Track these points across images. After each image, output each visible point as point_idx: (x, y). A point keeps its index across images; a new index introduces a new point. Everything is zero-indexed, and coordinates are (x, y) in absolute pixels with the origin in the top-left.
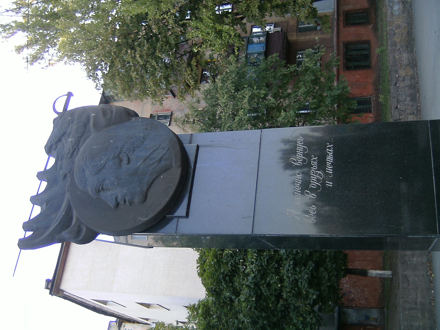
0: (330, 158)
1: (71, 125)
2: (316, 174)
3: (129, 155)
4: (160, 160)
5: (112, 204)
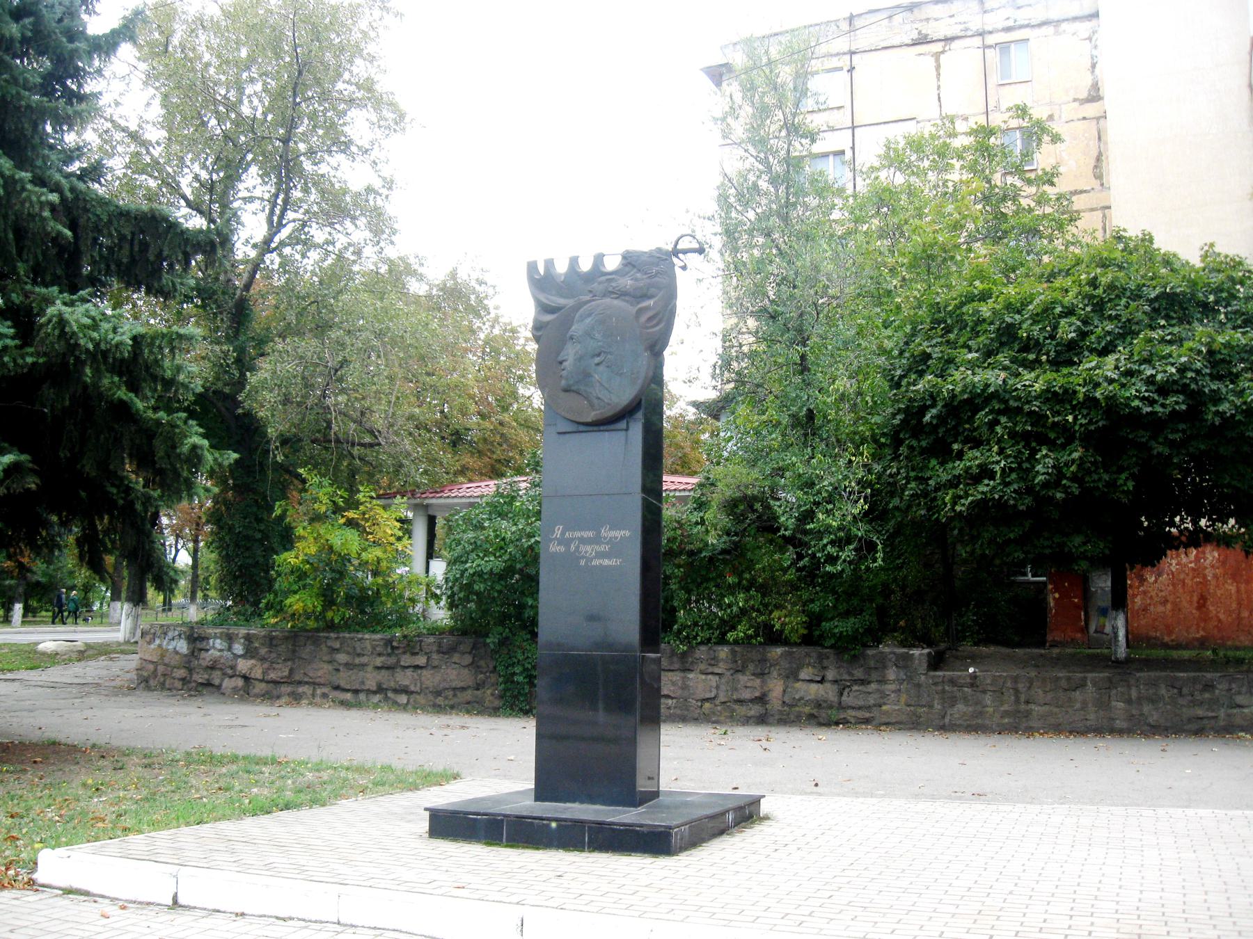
0: (606, 562)
5: (560, 359)
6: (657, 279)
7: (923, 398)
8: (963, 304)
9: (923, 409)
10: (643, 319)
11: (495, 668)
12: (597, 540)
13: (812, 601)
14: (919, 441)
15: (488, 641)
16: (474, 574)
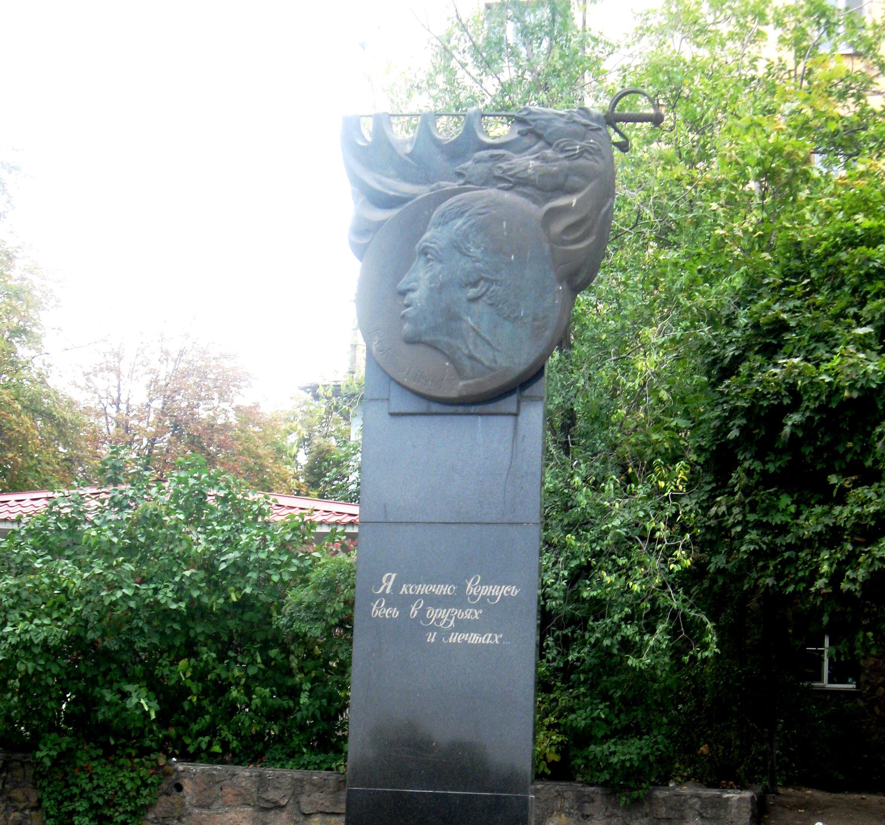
0: (475, 638)
1: (562, 156)
2: (450, 617)
3: (485, 298)
4: (471, 358)
5: (402, 286)
6: (581, 162)
7: (778, 393)
8: (837, 247)
9: (778, 413)
10: (557, 227)
11: (40, 801)
12: (459, 600)
13: (572, 710)
14: (764, 463)
15: (39, 754)
16: (14, 647)
